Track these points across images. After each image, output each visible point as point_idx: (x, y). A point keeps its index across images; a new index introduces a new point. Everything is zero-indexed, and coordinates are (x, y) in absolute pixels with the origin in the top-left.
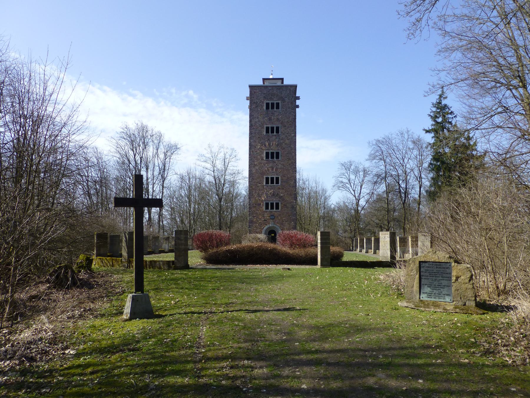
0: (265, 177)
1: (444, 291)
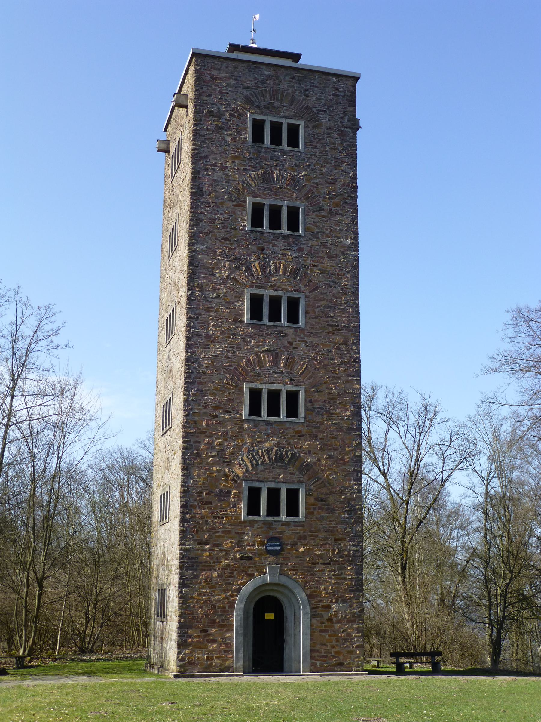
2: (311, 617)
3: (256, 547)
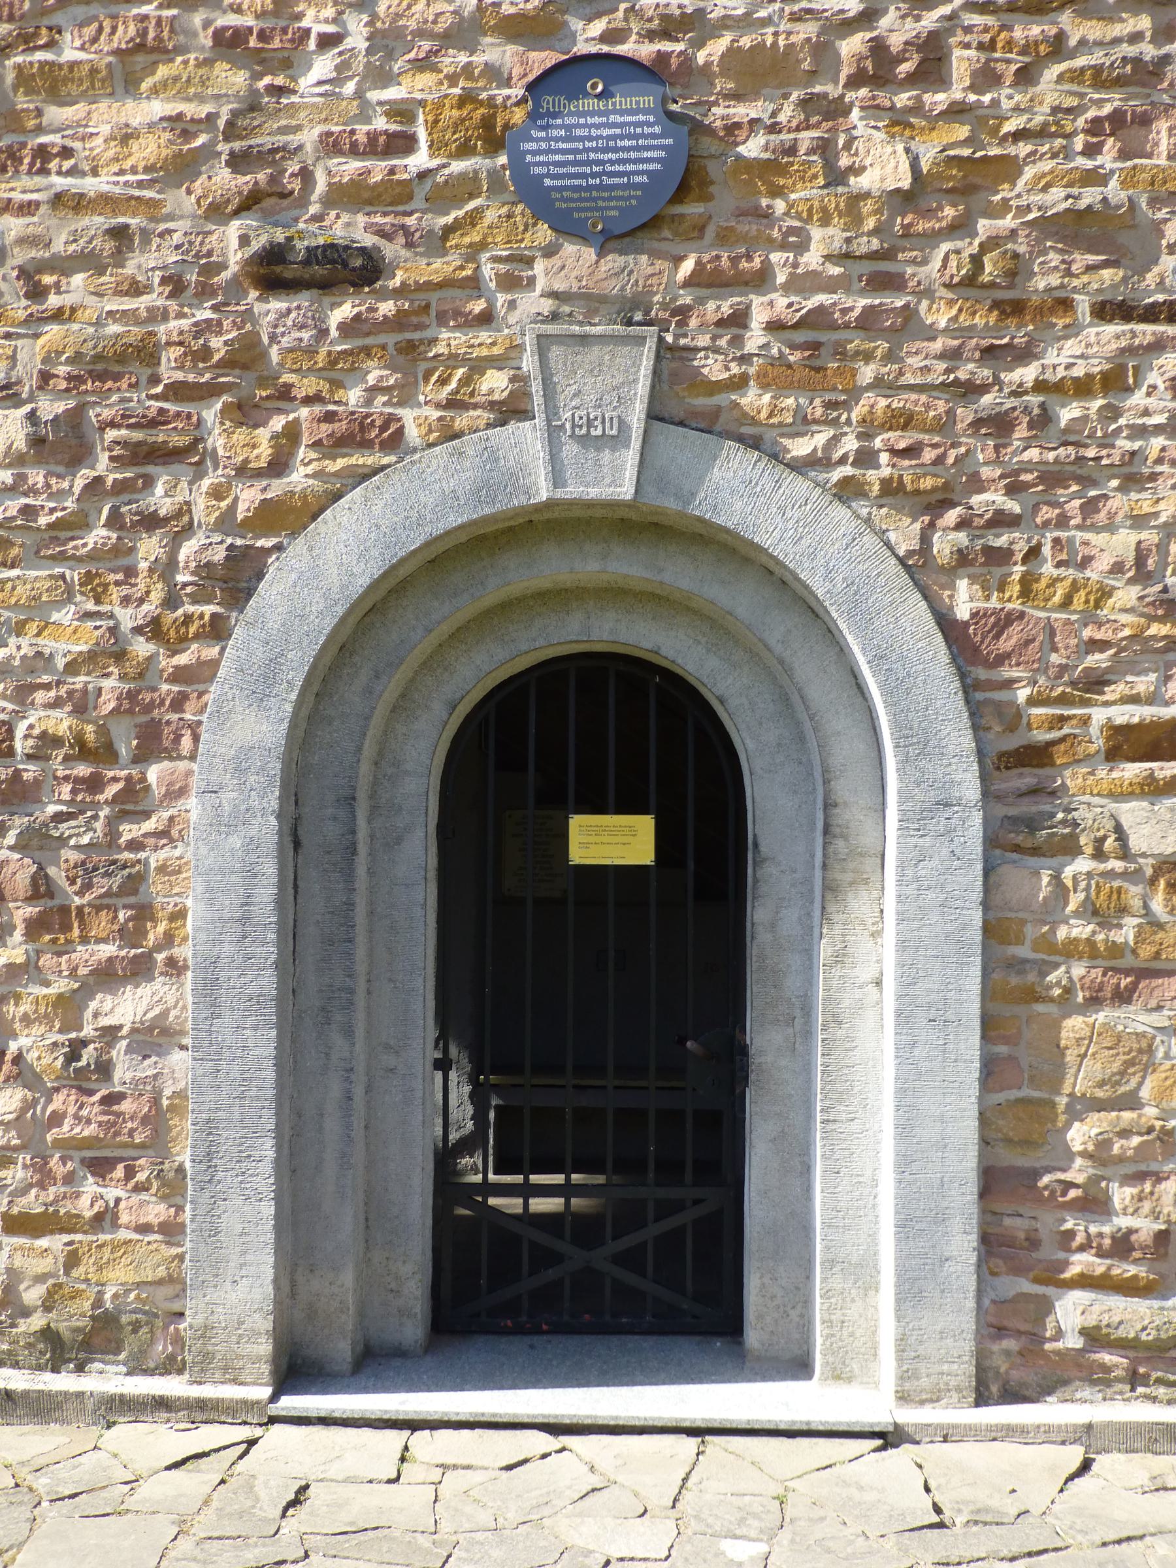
2: (991, 842)
3: (420, 159)
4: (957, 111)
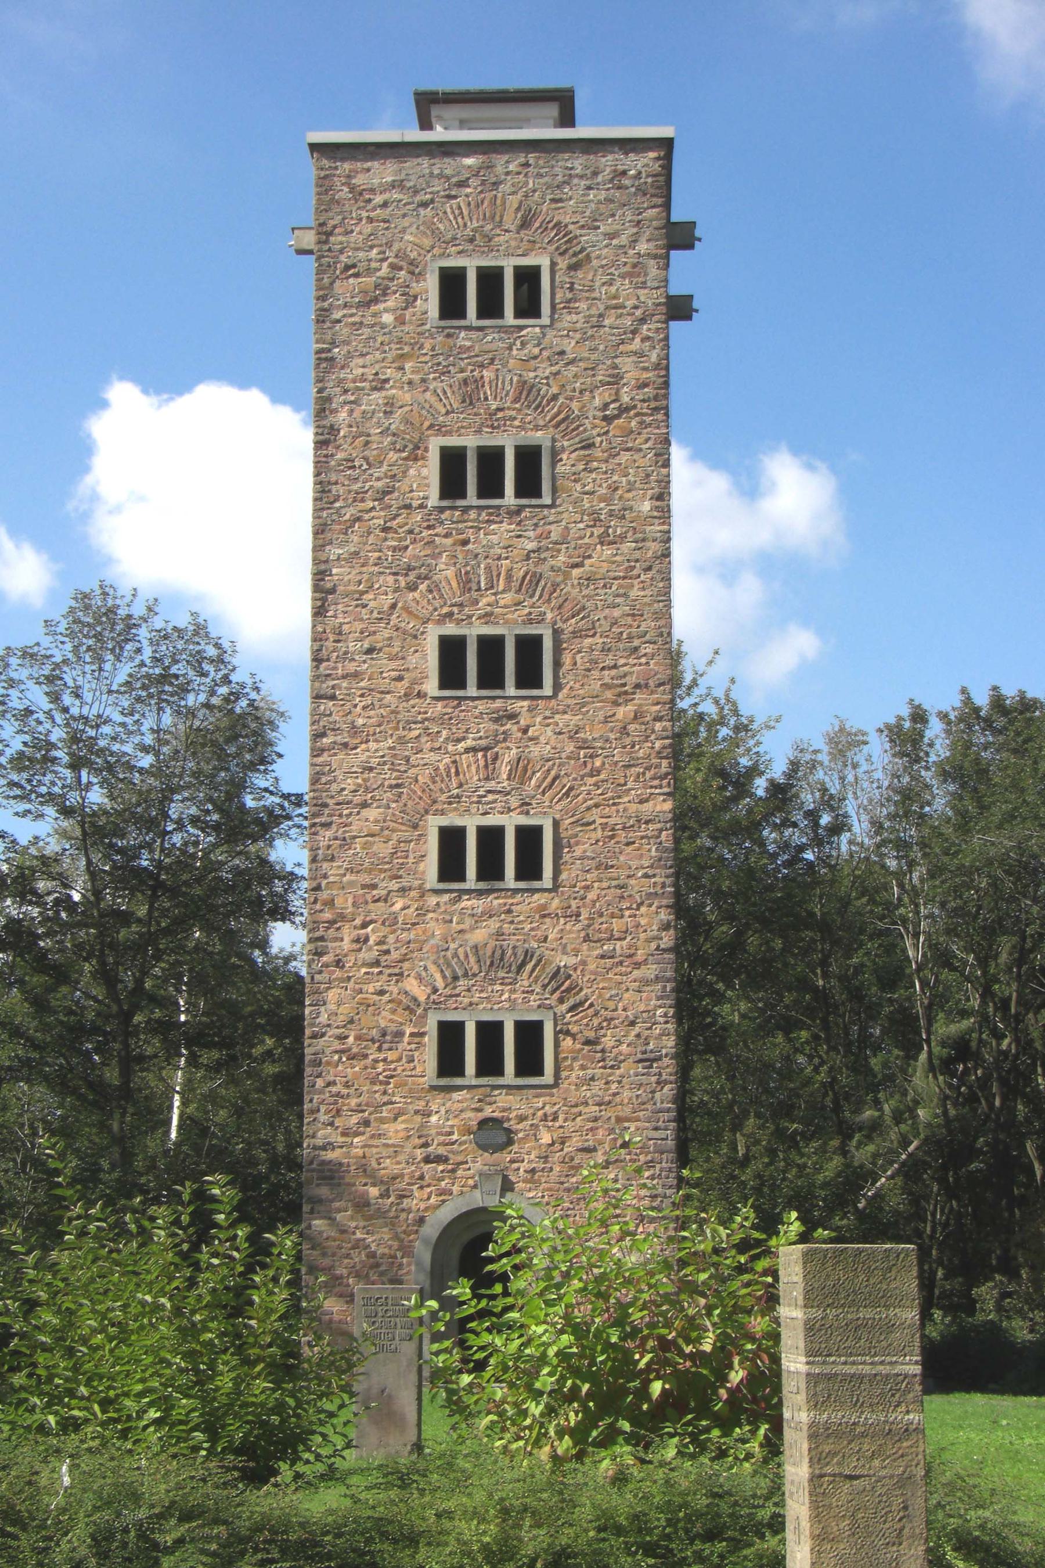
0: (434, 823)
1: (630, 1506)
4: (561, 1127)
